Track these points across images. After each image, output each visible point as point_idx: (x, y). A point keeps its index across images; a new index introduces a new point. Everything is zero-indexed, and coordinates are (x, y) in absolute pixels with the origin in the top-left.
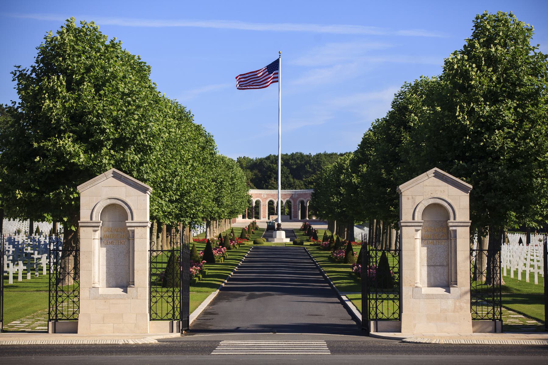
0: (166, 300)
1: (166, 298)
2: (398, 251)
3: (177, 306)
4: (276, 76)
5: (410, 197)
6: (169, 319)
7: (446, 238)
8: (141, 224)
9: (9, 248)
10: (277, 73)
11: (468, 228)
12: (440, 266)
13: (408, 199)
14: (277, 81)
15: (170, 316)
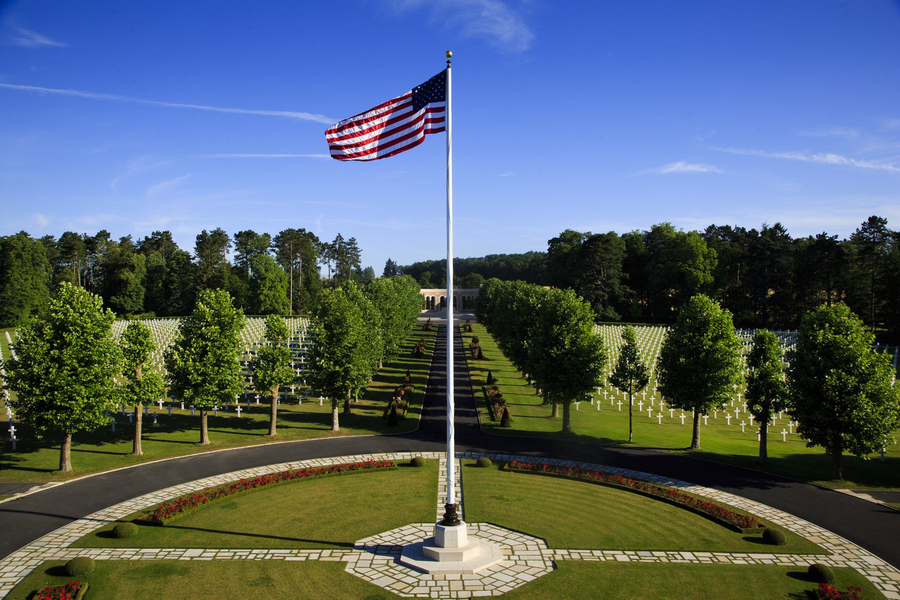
4: (438, 115)
9: (284, 309)
10: (443, 109)
14: (442, 129)
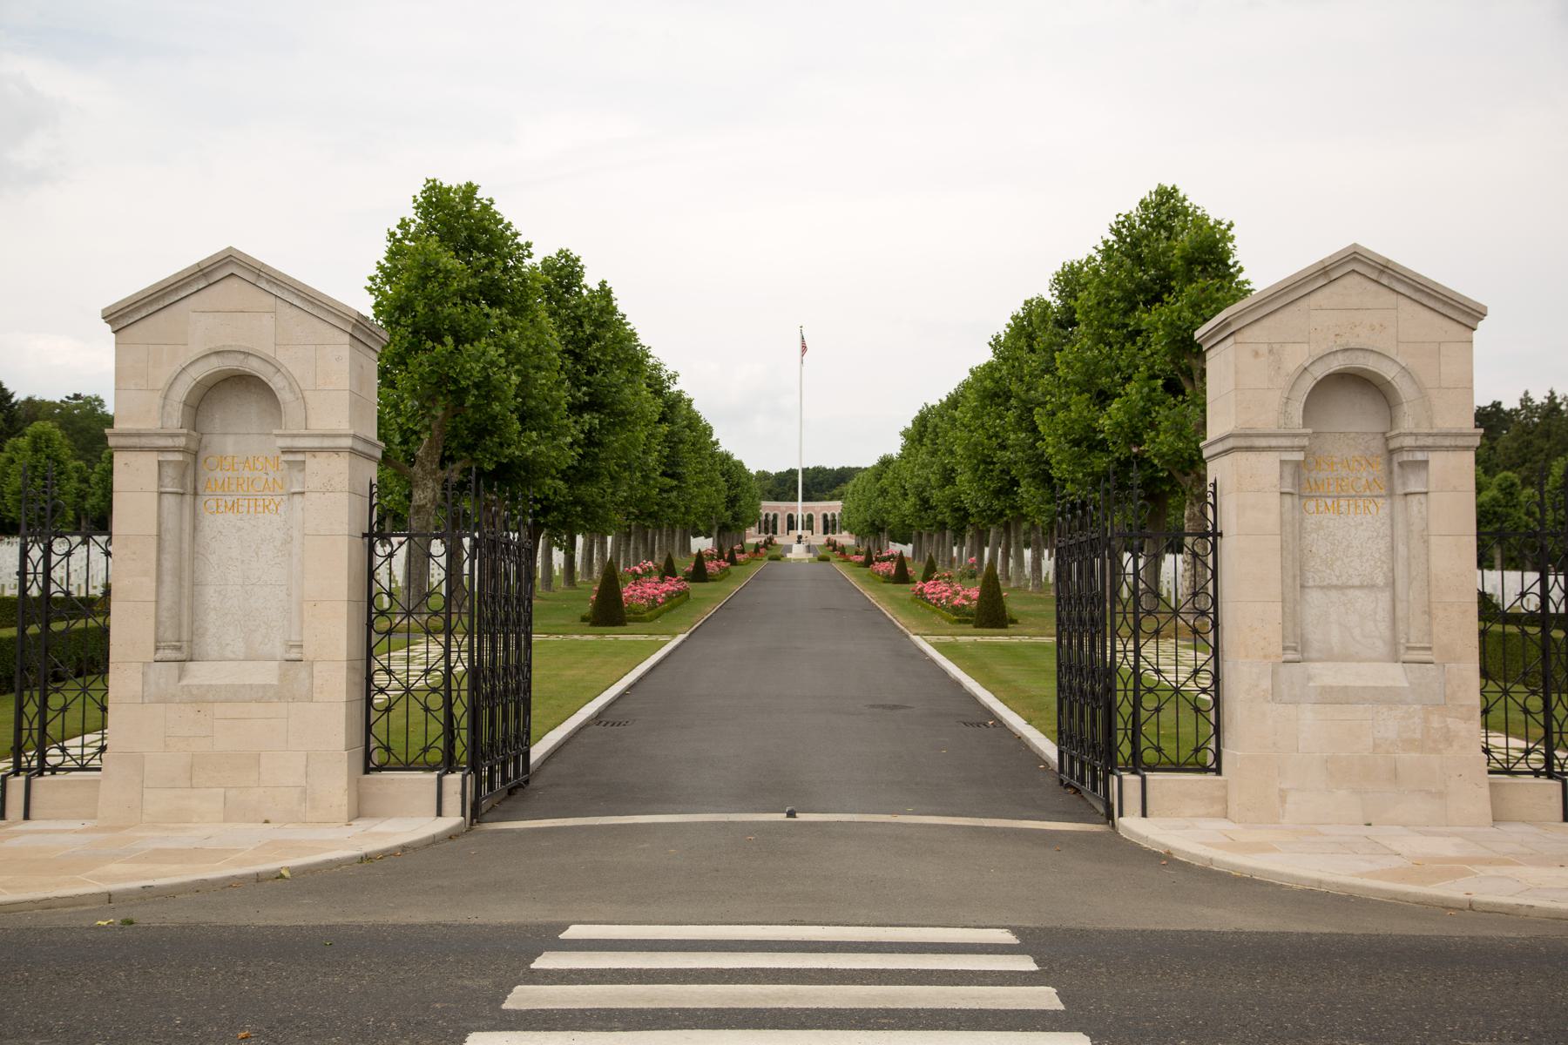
0: (422, 701)
2: (1211, 538)
5: (1264, 349)
6: (429, 768)
7: (1383, 492)
8: (327, 443)
11: (1470, 457)
12: (1361, 587)
13: (1256, 354)
15: (435, 756)
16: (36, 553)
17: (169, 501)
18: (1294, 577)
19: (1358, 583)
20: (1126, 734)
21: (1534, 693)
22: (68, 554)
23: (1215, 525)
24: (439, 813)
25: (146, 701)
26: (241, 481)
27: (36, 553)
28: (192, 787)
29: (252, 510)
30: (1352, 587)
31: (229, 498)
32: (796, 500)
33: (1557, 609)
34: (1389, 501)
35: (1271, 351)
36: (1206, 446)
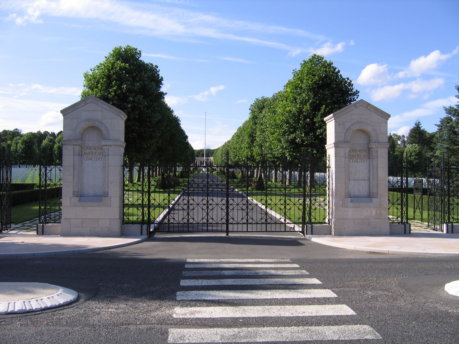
1: (298, 206)
2: (328, 168)
3: (145, 213)
5: (341, 123)
16: (43, 170)
17: (76, 157)
18: (348, 178)
19: (361, 179)
20: (308, 215)
21: (153, 204)
22: (51, 170)
23: (329, 165)
24: (142, 234)
25: (71, 206)
26: (92, 153)
27: (43, 170)
28: (82, 227)
29: (95, 160)
30: (360, 180)
31: (89, 157)
32: (204, 157)
33: (146, 168)
34: (369, 160)
35: (343, 124)
36: (327, 146)
